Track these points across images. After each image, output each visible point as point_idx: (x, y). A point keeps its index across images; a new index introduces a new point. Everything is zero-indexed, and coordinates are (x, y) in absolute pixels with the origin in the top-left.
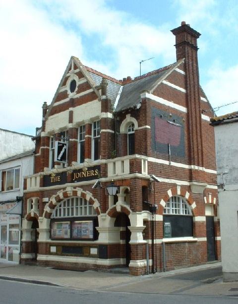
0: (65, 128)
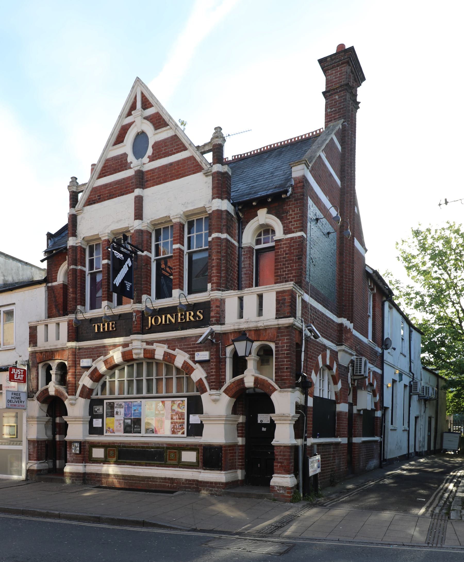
0: (203, 210)
